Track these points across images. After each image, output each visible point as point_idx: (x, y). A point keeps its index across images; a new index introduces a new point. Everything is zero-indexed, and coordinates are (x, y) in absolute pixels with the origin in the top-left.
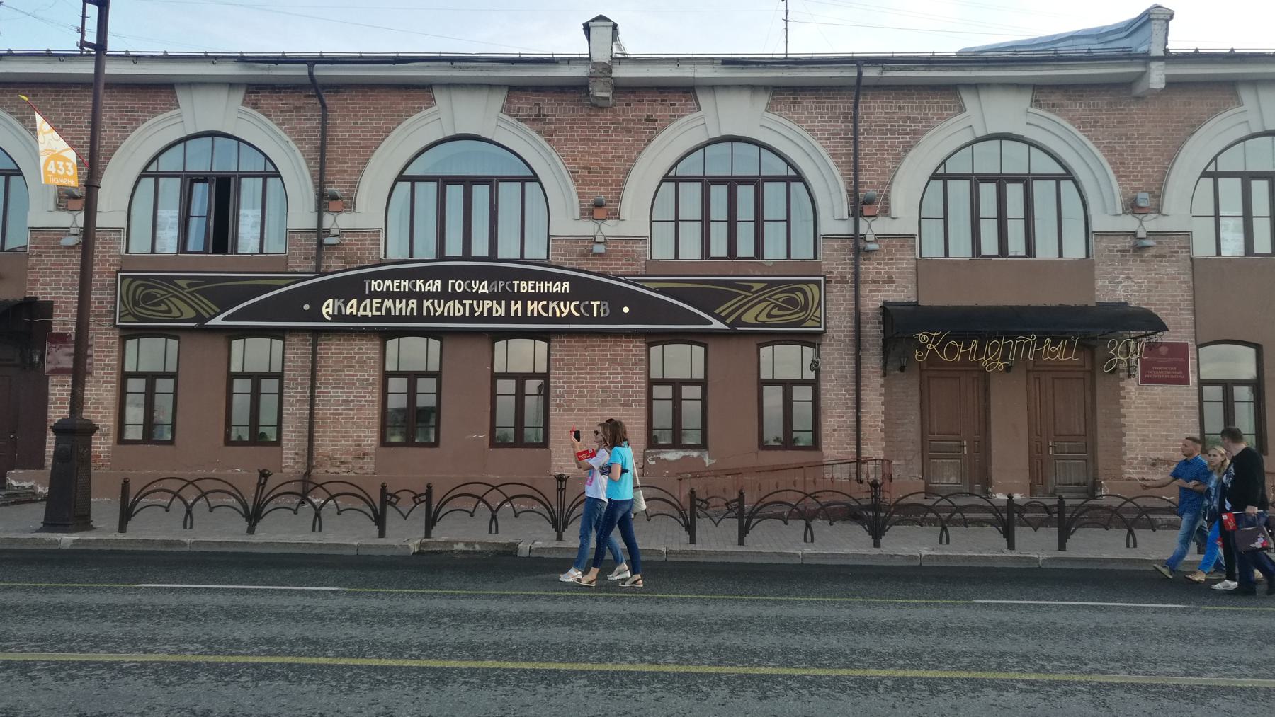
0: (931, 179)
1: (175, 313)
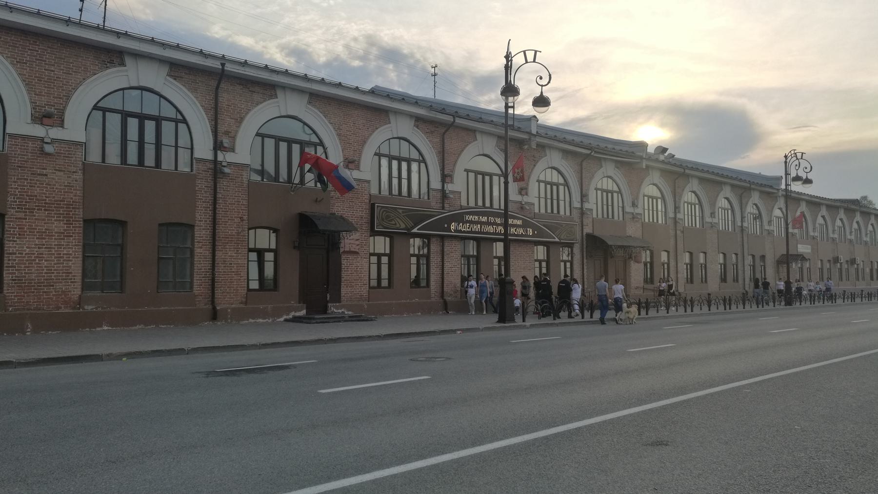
1: (398, 226)
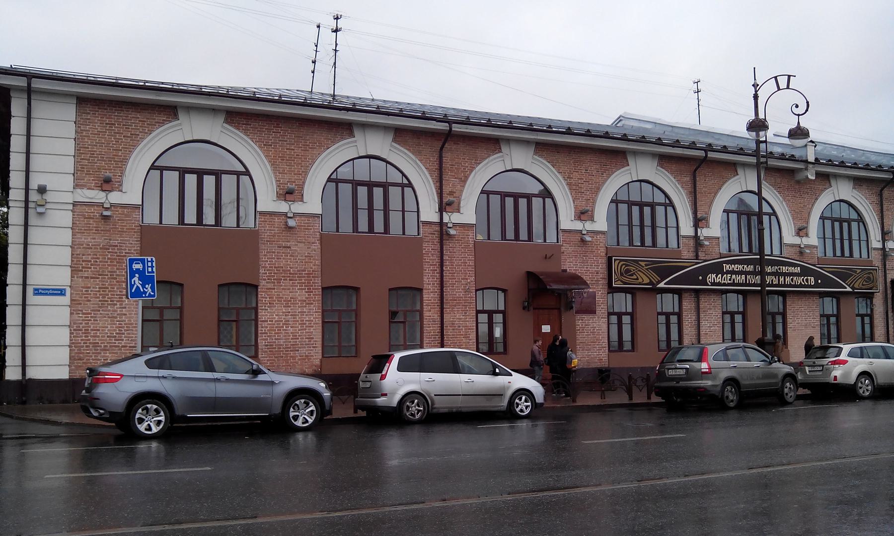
0: (150, 169)
1: (640, 280)
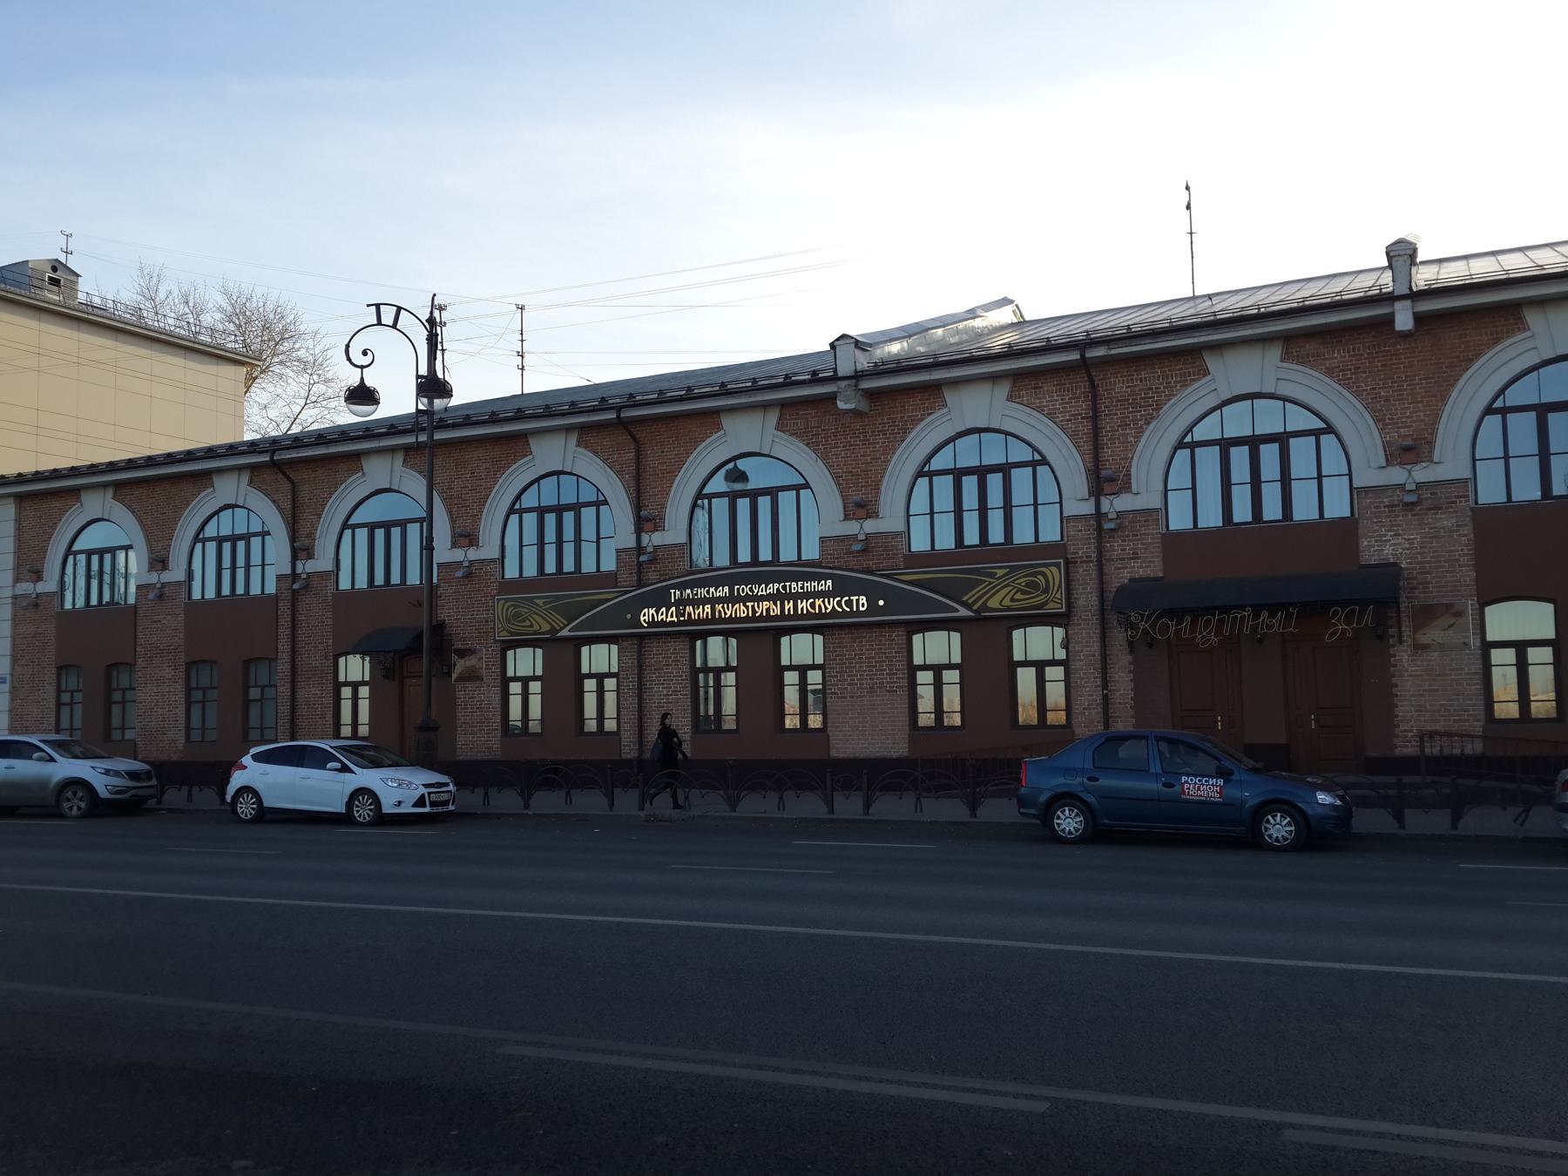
0: (1176, 449)
1: (536, 627)
